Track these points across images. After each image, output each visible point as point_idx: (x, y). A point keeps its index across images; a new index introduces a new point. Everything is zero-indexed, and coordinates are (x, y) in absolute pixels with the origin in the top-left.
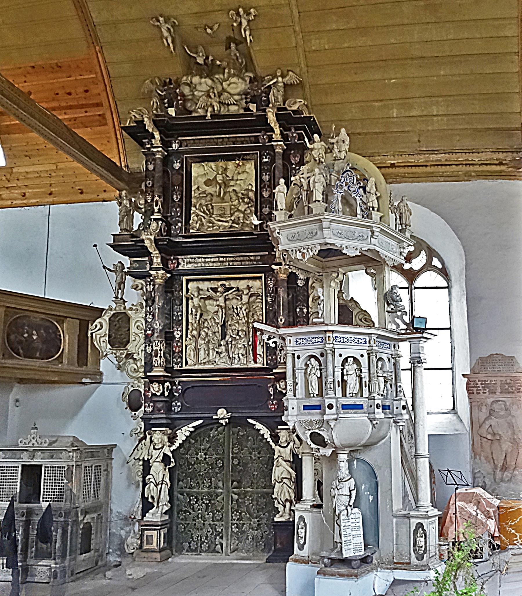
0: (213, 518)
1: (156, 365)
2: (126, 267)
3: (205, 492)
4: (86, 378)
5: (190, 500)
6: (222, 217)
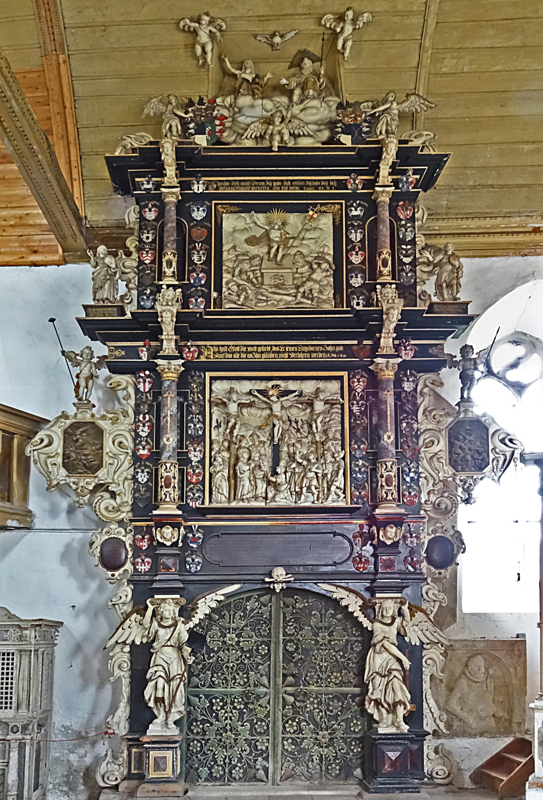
0: (251, 730)
1: (168, 499)
2: (95, 355)
3: (238, 692)
4: (13, 520)
5: (212, 704)
6: (280, 289)
